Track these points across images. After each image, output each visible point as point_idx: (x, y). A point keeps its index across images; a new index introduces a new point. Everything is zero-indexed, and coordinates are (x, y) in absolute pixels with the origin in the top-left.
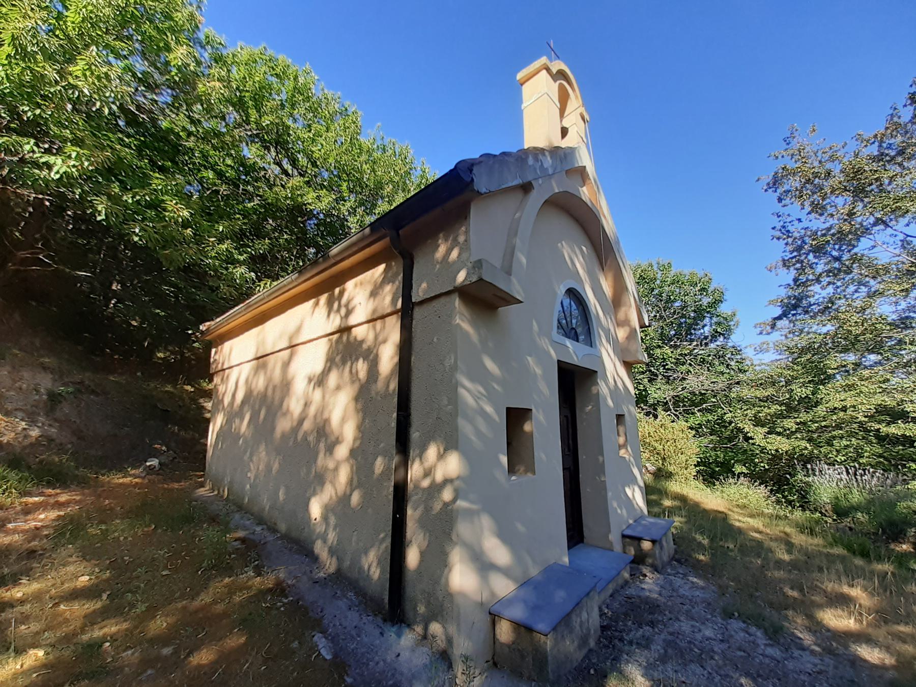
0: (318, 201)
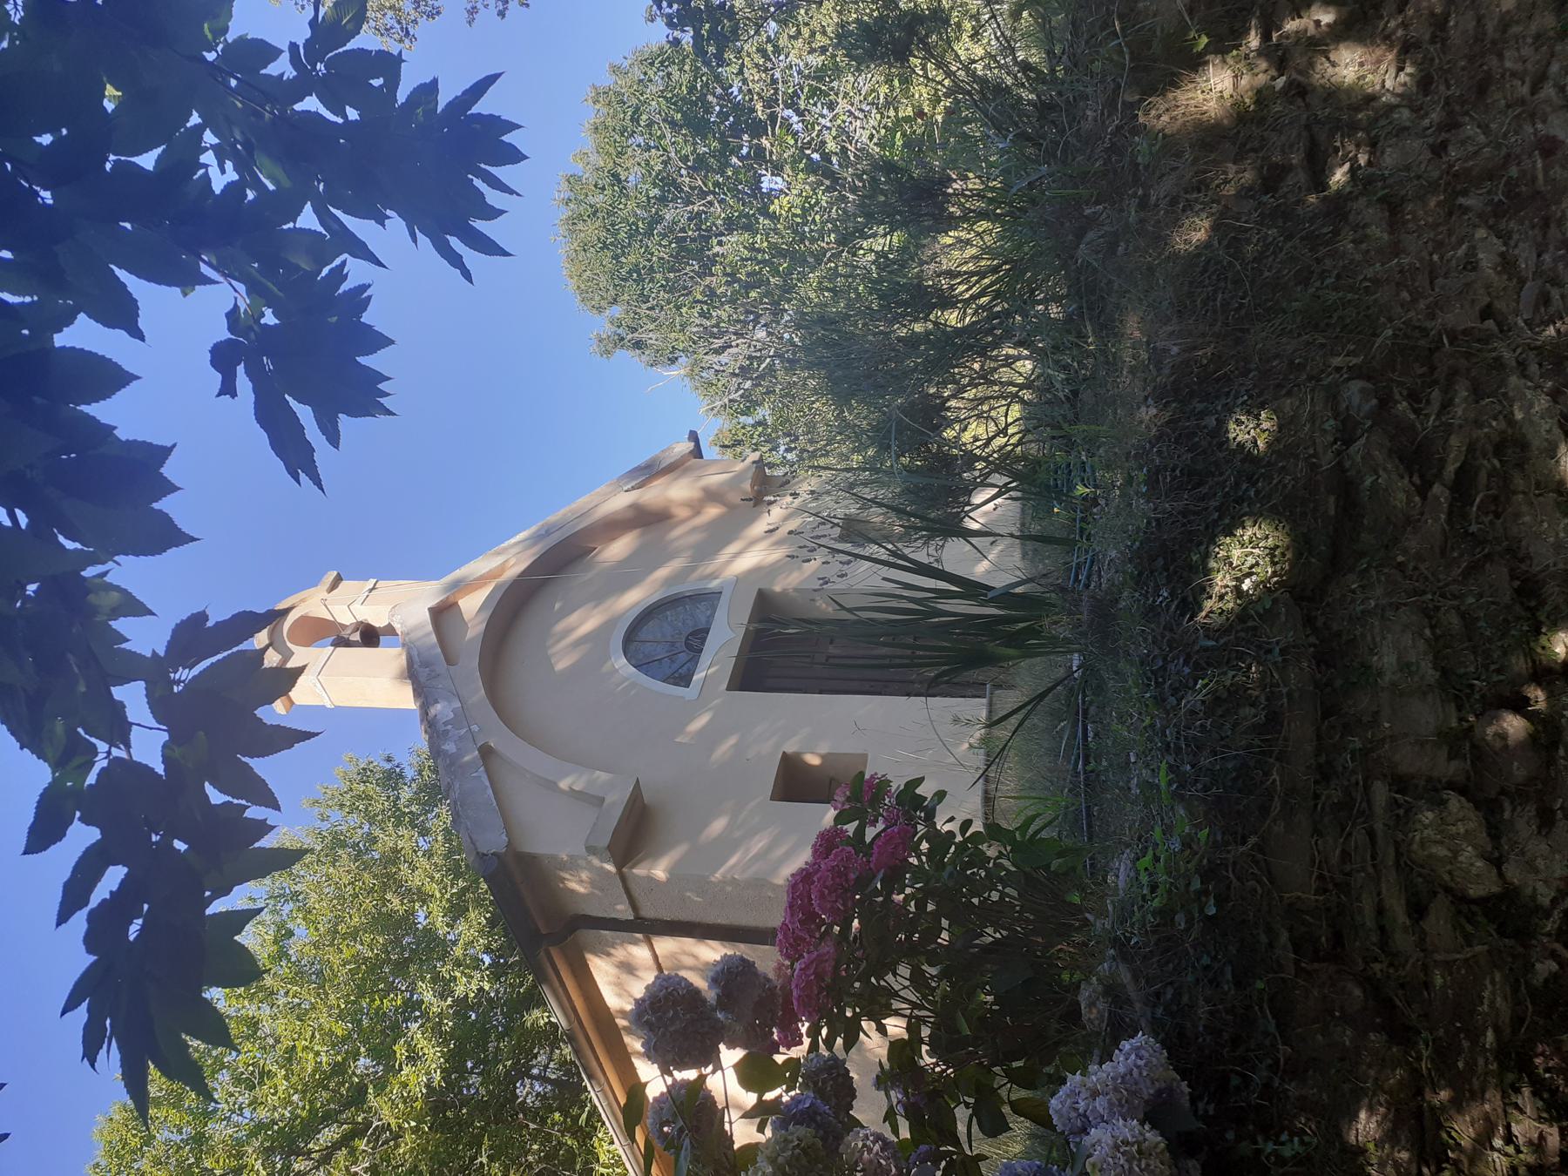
0: (423, 1066)
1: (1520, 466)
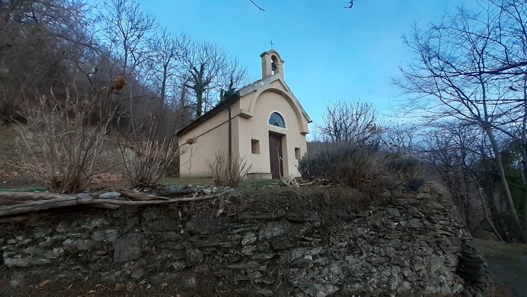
1: (308, 248)
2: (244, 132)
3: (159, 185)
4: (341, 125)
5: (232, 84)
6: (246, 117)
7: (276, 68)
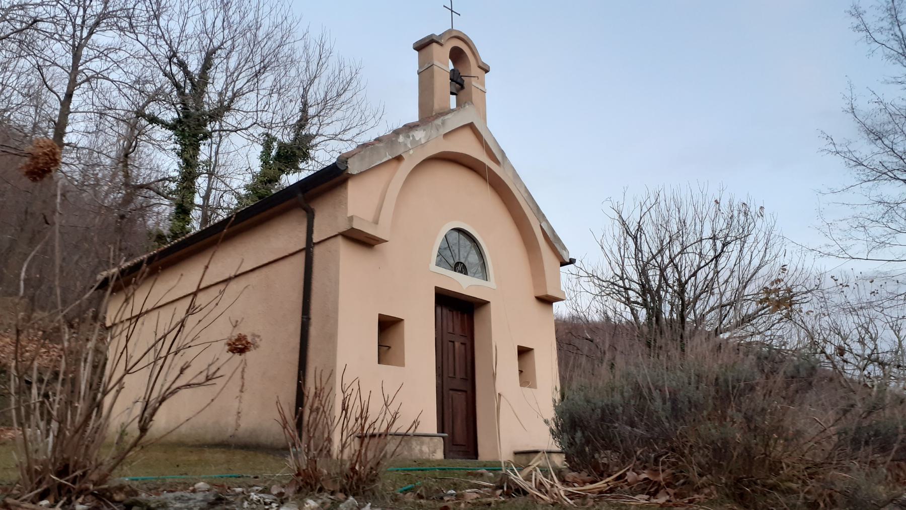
2: (357, 292)
3: (121, 488)
4: (662, 270)
5: (303, 123)
6: (363, 241)
7: (462, 87)
